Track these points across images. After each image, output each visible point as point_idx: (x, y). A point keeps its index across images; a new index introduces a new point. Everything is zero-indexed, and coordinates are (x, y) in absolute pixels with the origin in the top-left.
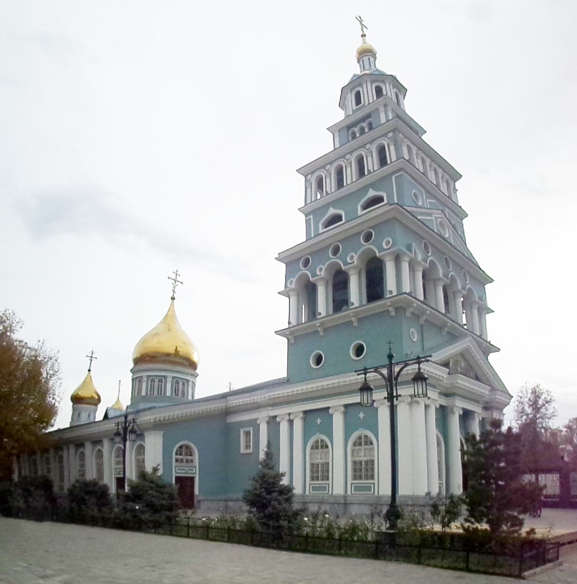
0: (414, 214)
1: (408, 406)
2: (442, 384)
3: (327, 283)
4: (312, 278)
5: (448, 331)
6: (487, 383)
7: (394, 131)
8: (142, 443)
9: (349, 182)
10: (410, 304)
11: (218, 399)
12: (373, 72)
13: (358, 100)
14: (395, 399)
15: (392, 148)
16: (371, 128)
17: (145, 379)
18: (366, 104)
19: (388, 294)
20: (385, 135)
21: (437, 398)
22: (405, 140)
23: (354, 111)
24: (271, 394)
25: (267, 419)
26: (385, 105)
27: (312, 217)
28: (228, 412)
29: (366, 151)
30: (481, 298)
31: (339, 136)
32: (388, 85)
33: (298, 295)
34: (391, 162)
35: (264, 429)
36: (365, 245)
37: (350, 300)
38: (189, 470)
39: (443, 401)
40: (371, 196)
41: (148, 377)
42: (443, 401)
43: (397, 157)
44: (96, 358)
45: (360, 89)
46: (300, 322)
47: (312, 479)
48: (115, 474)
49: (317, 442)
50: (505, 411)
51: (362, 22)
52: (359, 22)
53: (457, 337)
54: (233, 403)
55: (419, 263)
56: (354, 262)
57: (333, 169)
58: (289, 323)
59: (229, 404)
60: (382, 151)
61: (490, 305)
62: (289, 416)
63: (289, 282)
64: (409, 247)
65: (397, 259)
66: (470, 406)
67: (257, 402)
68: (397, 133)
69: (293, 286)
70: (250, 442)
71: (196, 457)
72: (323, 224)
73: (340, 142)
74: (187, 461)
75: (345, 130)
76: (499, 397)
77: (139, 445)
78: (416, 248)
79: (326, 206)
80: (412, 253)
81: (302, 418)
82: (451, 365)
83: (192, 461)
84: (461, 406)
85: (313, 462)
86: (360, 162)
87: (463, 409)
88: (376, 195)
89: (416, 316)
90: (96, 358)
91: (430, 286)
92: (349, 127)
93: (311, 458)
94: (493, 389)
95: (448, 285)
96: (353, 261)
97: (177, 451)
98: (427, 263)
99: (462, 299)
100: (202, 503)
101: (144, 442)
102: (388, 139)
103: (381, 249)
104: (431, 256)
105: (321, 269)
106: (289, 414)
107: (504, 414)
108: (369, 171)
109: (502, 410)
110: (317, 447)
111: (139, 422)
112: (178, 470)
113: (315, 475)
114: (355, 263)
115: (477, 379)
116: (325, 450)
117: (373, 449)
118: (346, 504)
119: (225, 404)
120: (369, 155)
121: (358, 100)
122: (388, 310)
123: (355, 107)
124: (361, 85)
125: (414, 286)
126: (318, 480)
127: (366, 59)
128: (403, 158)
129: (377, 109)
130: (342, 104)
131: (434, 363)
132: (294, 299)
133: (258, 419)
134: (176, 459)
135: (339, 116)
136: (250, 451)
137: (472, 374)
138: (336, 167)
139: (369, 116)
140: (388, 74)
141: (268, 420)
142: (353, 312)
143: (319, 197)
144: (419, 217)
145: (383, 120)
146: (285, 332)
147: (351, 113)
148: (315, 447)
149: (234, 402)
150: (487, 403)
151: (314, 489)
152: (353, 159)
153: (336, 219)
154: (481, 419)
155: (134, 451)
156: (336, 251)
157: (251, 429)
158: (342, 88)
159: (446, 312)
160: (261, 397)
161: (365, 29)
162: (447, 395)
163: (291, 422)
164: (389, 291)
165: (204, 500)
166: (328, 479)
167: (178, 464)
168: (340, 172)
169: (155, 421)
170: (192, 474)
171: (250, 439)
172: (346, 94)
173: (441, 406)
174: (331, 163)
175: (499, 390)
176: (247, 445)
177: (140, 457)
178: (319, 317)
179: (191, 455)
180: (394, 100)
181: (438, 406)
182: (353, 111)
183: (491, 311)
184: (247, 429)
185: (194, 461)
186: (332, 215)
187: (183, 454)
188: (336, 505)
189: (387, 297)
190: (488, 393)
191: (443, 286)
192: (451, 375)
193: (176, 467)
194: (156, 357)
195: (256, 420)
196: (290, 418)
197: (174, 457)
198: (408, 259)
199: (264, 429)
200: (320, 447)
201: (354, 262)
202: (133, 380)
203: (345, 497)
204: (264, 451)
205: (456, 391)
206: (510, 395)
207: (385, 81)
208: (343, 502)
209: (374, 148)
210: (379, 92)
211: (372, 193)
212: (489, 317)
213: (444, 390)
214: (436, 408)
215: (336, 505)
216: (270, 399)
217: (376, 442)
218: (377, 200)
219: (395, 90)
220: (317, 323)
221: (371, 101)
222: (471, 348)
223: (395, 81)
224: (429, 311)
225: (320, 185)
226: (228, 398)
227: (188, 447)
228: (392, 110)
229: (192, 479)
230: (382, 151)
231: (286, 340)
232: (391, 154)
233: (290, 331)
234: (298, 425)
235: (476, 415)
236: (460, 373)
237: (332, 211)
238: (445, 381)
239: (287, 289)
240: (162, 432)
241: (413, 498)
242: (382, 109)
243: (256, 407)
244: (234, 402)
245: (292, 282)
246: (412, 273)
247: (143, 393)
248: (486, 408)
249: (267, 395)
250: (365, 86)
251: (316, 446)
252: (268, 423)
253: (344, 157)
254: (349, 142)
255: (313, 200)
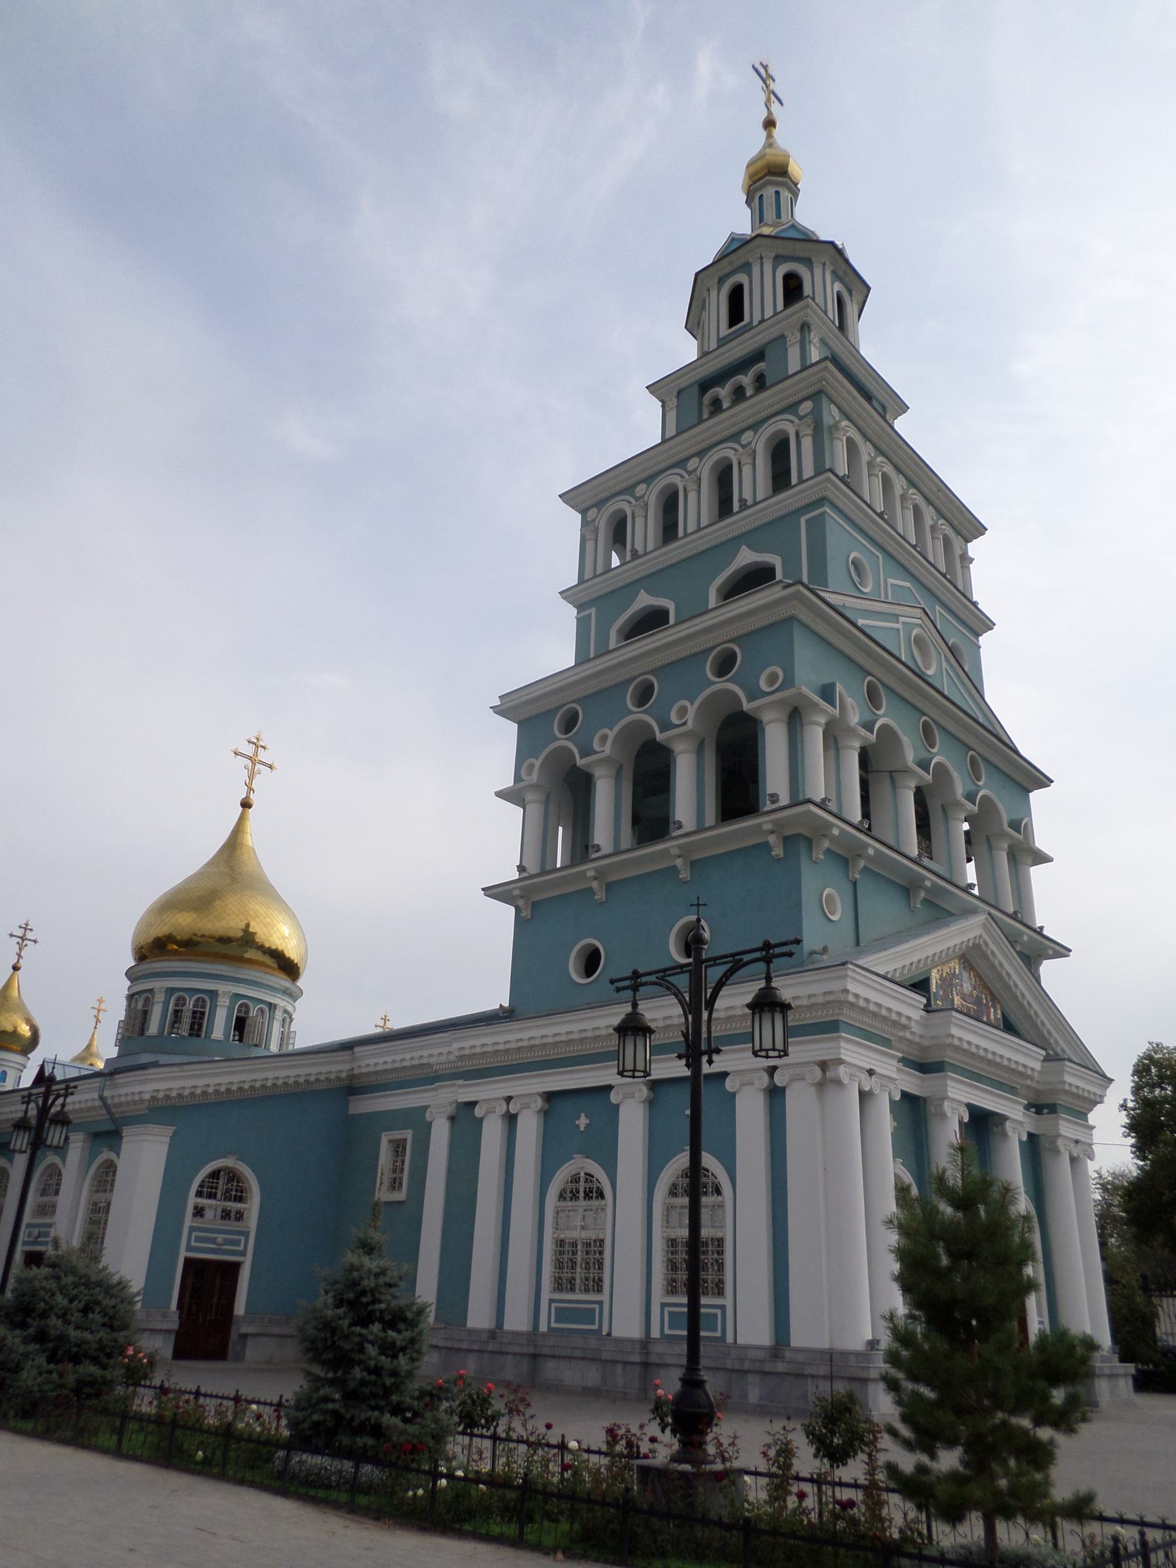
0: (847, 613)
1: (813, 1090)
2: (908, 1035)
3: (619, 771)
4: (581, 758)
5: (924, 898)
6: (1038, 1042)
7: (816, 396)
8: (113, 1156)
9: (691, 528)
10: (823, 830)
11: (326, 1052)
12: (782, 231)
13: (736, 313)
14: (705, 1058)
15: (807, 444)
16: (761, 383)
17: (160, 997)
18: (755, 323)
19: (768, 802)
20: (792, 408)
21: (894, 1075)
22: (844, 423)
23: (722, 342)
24: (467, 1044)
25: (450, 1110)
26: (805, 327)
27: (593, 611)
28: (352, 1087)
29: (740, 449)
30: (1016, 825)
31: (678, 407)
32: (818, 271)
33: (547, 802)
34: (801, 481)
35: (440, 1133)
36: (715, 683)
37: (674, 815)
38: (227, 1242)
39: (912, 1083)
40: (743, 563)
41: (170, 991)
42: (912, 1083)
43: (816, 468)
44: (35, 941)
45: (742, 278)
46: (548, 868)
47: (559, 1286)
48: (25, 1243)
49: (575, 1179)
50: (1093, 1117)
51: (769, 82)
52: (761, 83)
53: (950, 914)
54: (368, 1065)
55: (851, 731)
56: (685, 723)
57: (653, 495)
58: (521, 868)
59: (359, 1067)
60: (780, 453)
61: (1041, 842)
62: (508, 1103)
63: (525, 766)
64: (827, 693)
65: (795, 717)
66: (989, 1102)
67: (429, 1065)
68: (825, 400)
69: (534, 777)
70: (402, 1171)
71: (253, 1207)
72: (619, 631)
73: (678, 422)
74: (226, 1215)
75: (695, 390)
76: (1073, 1079)
77: (106, 1161)
78: (845, 694)
79: (631, 588)
80: (833, 704)
81: (539, 1112)
82: (933, 988)
83: (240, 1216)
84: (967, 1101)
85: (562, 1236)
86: (724, 477)
87: (969, 1106)
88: (756, 563)
89: (844, 859)
90: (35, 941)
91: (881, 789)
92: (705, 386)
93: (557, 1227)
94: (1053, 1057)
95: (929, 786)
96: (684, 720)
97: (201, 1186)
98: (873, 734)
99: (966, 826)
100: (250, 1342)
101: (118, 1154)
102: (801, 418)
103: (754, 694)
104: (883, 716)
105: (604, 739)
106: (509, 1099)
107: (1092, 1128)
108: (743, 501)
109: (1083, 1116)
110: (574, 1196)
111: (73, 1103)
112: (198, 1239)
113: (566, 1275)
114: (690, 725)
115: (1008, 1027)
116: (595, 1203)
117: (721, 1206)
118: (646, 1365)
119: (346, 1067)
120: (746, 460)
121: (736, 313)
122: (768, 842)
123: (725, 331)
124: (746, 267)
125: (839, 782)
126: (572, 1290)
127: (769, 192)
128: (831, 470)
129: (782, 337)
130: (694, 324)
131: (884, 977)
132: (535, 809)
133: (427, 1107)
134: (196, 1208)
135: (686, 351)
136: (401, 1196)
137: (994, 1014)
138: (662, 492)
139: (758, 356)
140: (823, 238)
141: (454, 1114)
142: (679, 846)
143: (615, 561)
144: (860, 622)
145: (794, 365)
146: (511, 891)
147: (713, 346)
148: (569, 1194)
149: (372, 1062)
150: (1038, 1093)
151: (562, 1315)
152: (705, 470)
153: (653, 620)
154: (1025, 1138)
155: (88, 1181)
156: (644, 695)
157: (408, 1135)
158: (697, 274)
159: (920, 855)
160: (420, 1053)
161: (775, 106)
162: (926, 1067)
163: (511, 1119)
164: (772, 795)
165: (256, 1335)
166: (599, 1290)
167: (199, 1222)
168: (670, 504)
169: (154, 1098)
170: (233, 1253)
171: (403, 1162)
172: (705, 294)
173: (905, 1095)
174: (648, 480)
175: (1071, 1061)
176: (395, 1179)
177: (101, 1196)
178: (594, 856)
179: (240, 1199)
180: (830, 315)
181: (897, 1097)
182: (719, 340)
183: (1041, 858)
184: (397, 1135)
185: (245, 1216)
186: (646, 607)
187: (219, 1196)
188: (619, 1367)
189: (765, 809)
190: (1037, 1066)
191: (914, 790)
192: (932, 1015)
193: (192, 1229)
194: (196, 944)
195: (425, 1108)
196: (508, 1110)
197: (192, 1200)
198: (823, 720)
199: (440, 1133)
200: (582, 1194)
201: (685, 723)
202: (131, 998)
203: (646, 1343)
204: (392, 1361)
205: (949, 1057)
206: (1104, 1076)
207: (813, 259)
208: (636, 1358)
209: (760, 443)
210: (793, 289)
211: (746, 557)
212: (1036, 873)
213: (914, 1054)
214: (892, 1102)
215: (619, 1367)
216: (461, 1058)
217: (731, 1189)
218: (758, 576)
219: (838, 286)
220: (589, 869)
221: (769, 313)
222: (986, 943)
223: (841, 261)
224: (873, 847)
225: (619, 534)
226: (357, 1049)
227: (233, 1176)
228: (822, 340)
229: (235, 1267)
230: (780, 453)
231: (512, 910)
232: (803, 460)
233: (521, 888)
234: (529, 1127)
235: (1008, 1124)
236: (957, 1011)
237: (644, 600)
238: (915, 1028)
239: (521, 785)
240: (169, 1130)
241: (830, 1356)
242: (793, 338)
243: (428, 1077)
244: (372, 1062)
245: (531, 767)
246: (832, 752)
247: (153, 1028)
248: (1041, 1107)
249: (456, 1046)
250: (756, 270)
251: (571, 1192)
252: (452, 1119)
253: (682, 463)
254: (701, 421)
255: (599, 570)
